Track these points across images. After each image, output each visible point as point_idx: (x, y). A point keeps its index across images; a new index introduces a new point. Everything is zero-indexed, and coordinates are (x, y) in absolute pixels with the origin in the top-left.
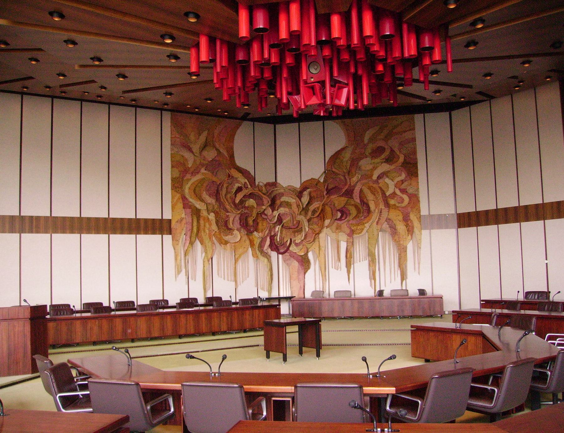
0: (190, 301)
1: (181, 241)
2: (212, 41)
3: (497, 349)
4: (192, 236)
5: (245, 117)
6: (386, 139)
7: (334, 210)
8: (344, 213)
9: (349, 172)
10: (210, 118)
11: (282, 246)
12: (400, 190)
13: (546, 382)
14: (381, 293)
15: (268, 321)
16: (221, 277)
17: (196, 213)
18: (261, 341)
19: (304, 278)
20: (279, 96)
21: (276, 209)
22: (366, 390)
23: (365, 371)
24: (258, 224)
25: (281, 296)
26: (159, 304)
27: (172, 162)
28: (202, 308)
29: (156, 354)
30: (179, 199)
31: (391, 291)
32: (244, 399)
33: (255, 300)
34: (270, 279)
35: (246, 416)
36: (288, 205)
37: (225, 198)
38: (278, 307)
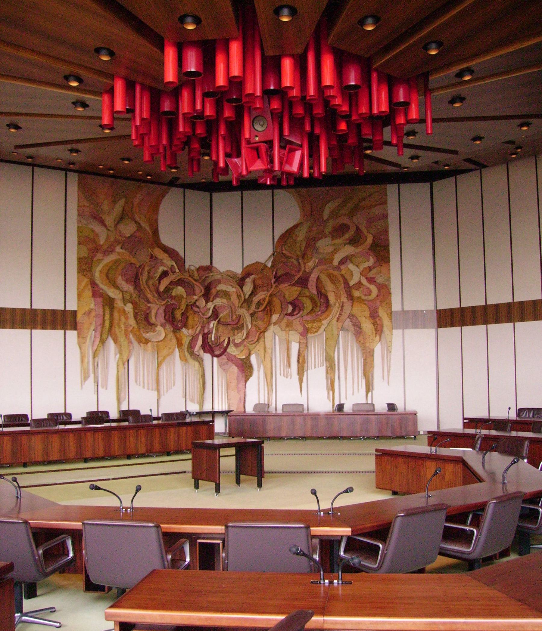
0: (100, 415)
1: (88, 338)
2: (130, 86)
3: (480, 480)
4: (104, 332)
5: (173, 183)
6: (351, 215)
7: (284, 303)
8: (296, 306)
9: (304, 255)
10: (128, 182)
11: (217, 346)
12: (367, 278)
13: (537, 522)
14: (340, 407)
15: (197, 441)
16: (140, 385)
17: (109, 303)
18: (188, 466)
19: (245, 387)
20: (214, 158)
21: (211, 299)
22: (315, 531)
23: (313, 507)
24: (187, 318)
25: (216, 409)
26: (59, 418)
27: (79, 237)
28: (114, 424)
29: (46, 482)
30: (87, 285)
31: (353, 405)
32: (162, 541)
33: (183, 415)
34: (202, 388)
35: (164, 564)
36: (226, 294)
37: (146, 284)
38: (211, 424)
